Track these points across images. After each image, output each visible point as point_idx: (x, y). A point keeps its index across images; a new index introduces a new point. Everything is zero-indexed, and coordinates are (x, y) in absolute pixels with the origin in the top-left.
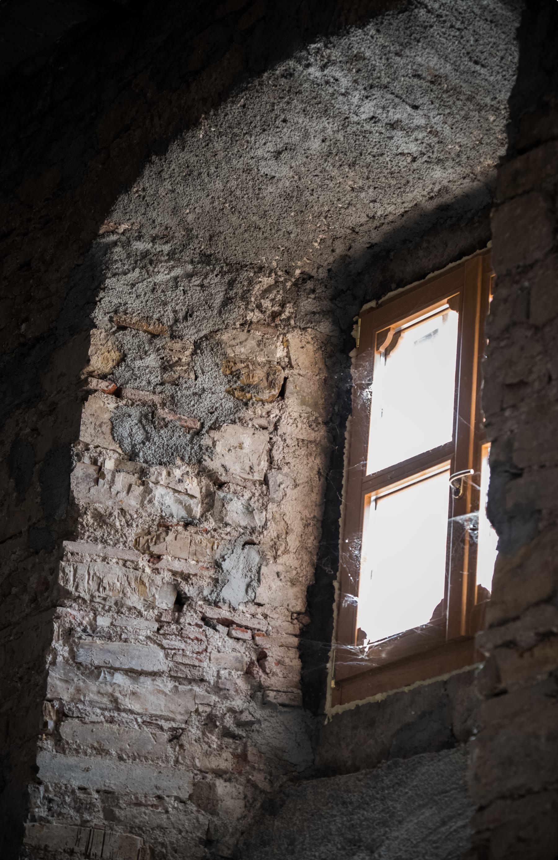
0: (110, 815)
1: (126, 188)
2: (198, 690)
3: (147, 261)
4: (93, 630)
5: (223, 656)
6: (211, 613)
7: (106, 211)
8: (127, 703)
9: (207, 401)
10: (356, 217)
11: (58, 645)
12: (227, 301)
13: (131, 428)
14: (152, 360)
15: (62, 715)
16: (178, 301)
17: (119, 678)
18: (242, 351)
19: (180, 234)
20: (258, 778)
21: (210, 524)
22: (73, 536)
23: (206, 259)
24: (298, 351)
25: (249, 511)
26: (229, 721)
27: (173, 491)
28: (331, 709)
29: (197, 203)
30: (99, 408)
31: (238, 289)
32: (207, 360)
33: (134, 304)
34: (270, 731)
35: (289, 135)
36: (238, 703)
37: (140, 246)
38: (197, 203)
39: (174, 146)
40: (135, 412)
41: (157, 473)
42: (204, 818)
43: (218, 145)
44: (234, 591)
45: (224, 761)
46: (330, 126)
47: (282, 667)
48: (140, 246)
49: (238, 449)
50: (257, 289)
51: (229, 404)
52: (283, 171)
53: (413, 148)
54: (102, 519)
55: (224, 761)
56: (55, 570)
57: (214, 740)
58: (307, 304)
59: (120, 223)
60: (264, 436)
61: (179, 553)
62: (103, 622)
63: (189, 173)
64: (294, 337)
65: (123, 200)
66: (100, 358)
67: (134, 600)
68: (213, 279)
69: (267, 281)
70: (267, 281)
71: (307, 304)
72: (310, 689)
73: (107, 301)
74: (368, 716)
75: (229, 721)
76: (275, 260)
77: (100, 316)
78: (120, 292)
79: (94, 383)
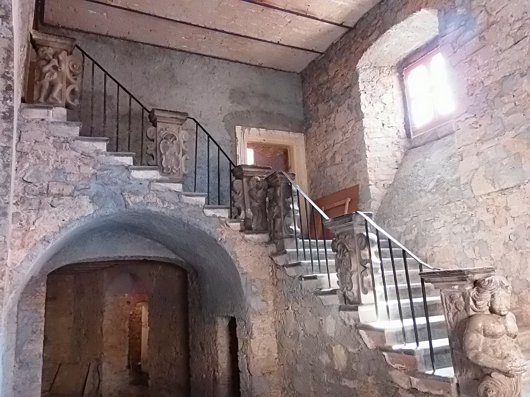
0: (380, 161)
1: (360, 58)
2: (389, 138)
3: (365, 70)
4: (370, 132)
5: (392, 132)
6: (389, 126)
7: (357, 63)
8: (379, 143)
9: (380, 91)
10: (401, 54)
11: (365, 135)
12: (380, 73)
13: (369, 98)
14: (370, 86)
15: (369, 147)
16: (372, 75)
17: (376, 139)
18: (384, 81)
19: (370, 64)
20: (403, 150)
21: (385, 111)
22: (363, 118)
23: (375, 67)
24: (394, 79)
25: (391, 108)
26: (396, 142)
27: (379, 107)
28: (412, 137)
29: (372, 58)
30: (363, 97)
31: (381, 71)
32: (378, 84)
33: (364, 78)
34: (403, 142)
35: (388, 43)
36: (396, 139)
37: (363, 68)
38: (372, 58)
39: (368, 49)
40: (369, 96)
41: (374, 104)
42: (395, 158)
43: (376, 47)
44: (392, 121)
45: (397, 149)
46: (47, 74)
47: (403, 132)
48: (363, 68)
49: (387, 98)
50: (385, 70)
51: (384, 91)
52: (387, 49)
53: (412, 40)
54: (367, 114)
55: (397, 149)
56: (362, 124)
57: (394, 145)
58: (394, 71)
59: (359, 65)
60: (391, 95)
61: (381, 117)
62: (372, 131)
63: (371, 53)
64: (393, 77)
65: (360, 60)
66: (361, 87)
67: (376, 126)
68: (377, 70)
69: (386, 68)
70: (386, 68)
71: (394, 71)
72: (408, 135)
73: (360, 78)
74: (421, 137)
75: (396, 142)
76: (387, 65)
77: (359, 81)
78: (362, 76)
79: (361, 92)
